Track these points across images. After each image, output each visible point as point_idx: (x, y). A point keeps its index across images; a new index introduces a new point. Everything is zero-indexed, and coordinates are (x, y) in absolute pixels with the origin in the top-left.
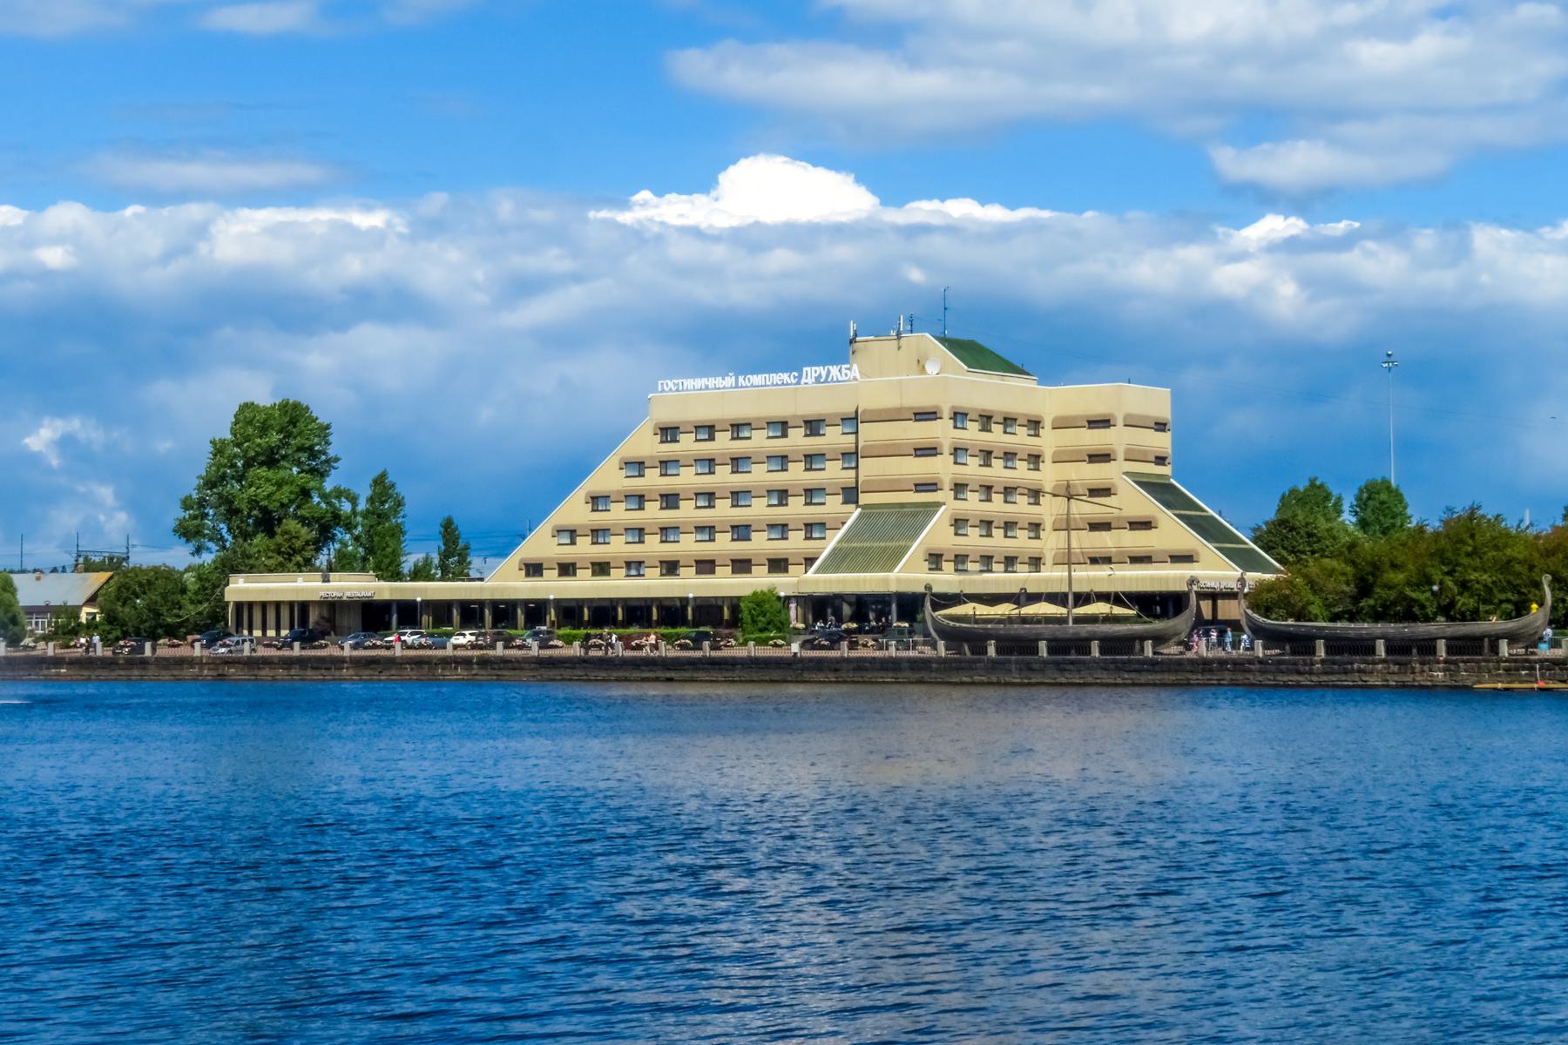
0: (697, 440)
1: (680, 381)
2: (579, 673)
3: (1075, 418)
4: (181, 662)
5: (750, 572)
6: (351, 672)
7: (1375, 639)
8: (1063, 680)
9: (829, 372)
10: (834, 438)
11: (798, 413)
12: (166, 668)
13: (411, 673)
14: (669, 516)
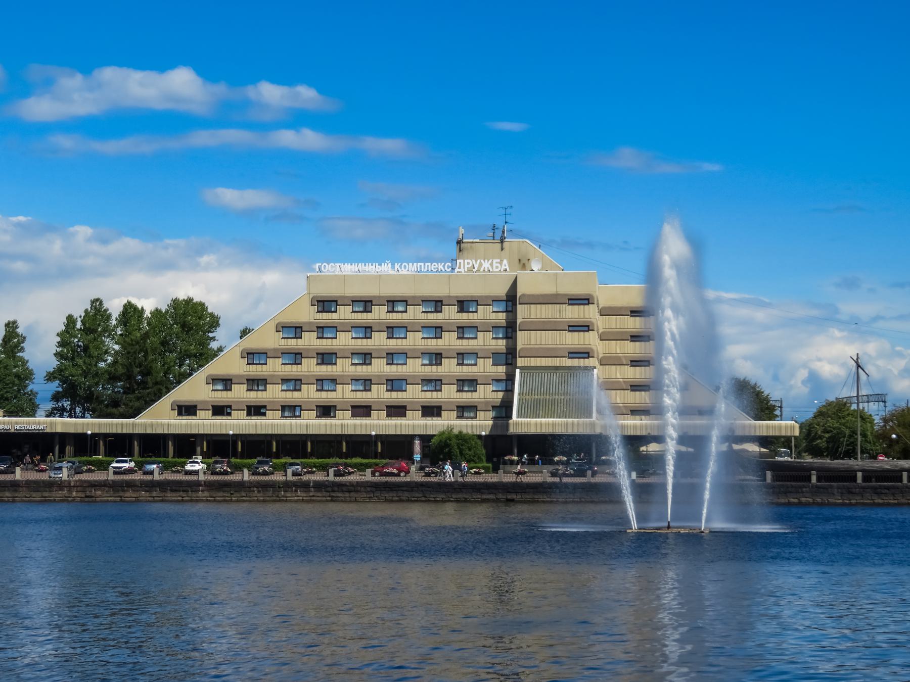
0: (353, 312)
3: (621, 308)
4: (51, 485)
5: (405, 416)
6: (206, 494)
7: (856, 471)
8: (880, 501)
9: (481, 265)
10: (379, 314)
11: (451, 295)
12: (36, 490)
13: (258, 495)
14: (325, 370)
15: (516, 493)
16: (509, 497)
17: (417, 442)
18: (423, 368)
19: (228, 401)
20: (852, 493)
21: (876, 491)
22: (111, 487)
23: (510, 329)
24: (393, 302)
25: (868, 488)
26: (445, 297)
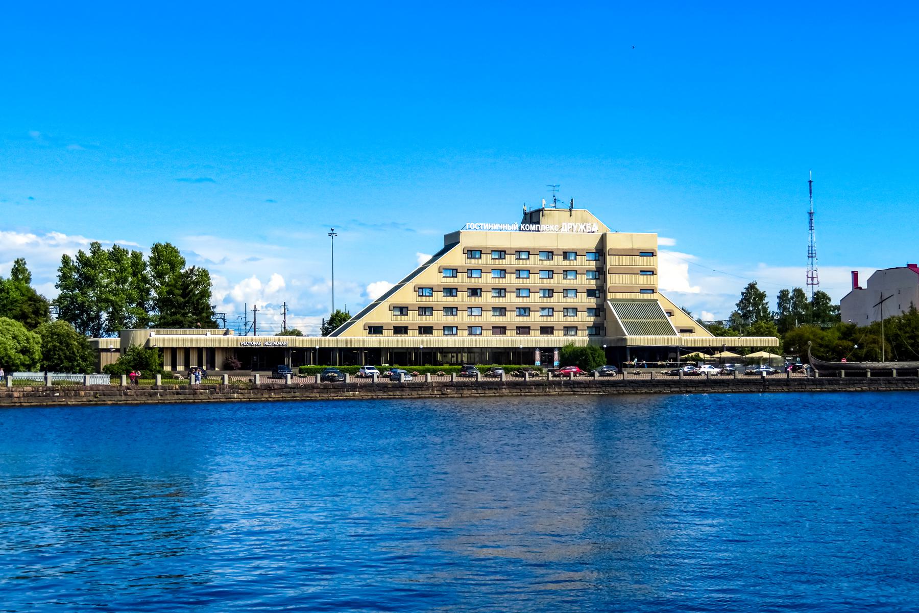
1: (482, 224)
2: (629, 389)
6: (507, 391)
8: (907, 388)
10: (558, 262)
12: (414, 390)
15: (692, 387)
16: (688, 390)
17: (537, 353)
18: (541, 300)
19: (405, 323)
20: (891, 383)
21: (904, 381)
22: (455, 386)
23: (600, 273)
24: (520, 252)
25: (900, 380)
26: (555, 249)
